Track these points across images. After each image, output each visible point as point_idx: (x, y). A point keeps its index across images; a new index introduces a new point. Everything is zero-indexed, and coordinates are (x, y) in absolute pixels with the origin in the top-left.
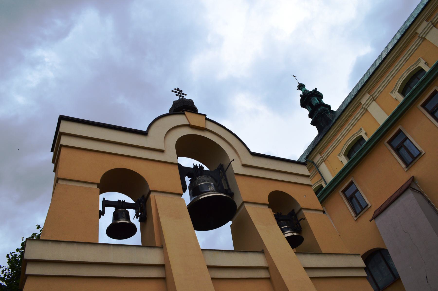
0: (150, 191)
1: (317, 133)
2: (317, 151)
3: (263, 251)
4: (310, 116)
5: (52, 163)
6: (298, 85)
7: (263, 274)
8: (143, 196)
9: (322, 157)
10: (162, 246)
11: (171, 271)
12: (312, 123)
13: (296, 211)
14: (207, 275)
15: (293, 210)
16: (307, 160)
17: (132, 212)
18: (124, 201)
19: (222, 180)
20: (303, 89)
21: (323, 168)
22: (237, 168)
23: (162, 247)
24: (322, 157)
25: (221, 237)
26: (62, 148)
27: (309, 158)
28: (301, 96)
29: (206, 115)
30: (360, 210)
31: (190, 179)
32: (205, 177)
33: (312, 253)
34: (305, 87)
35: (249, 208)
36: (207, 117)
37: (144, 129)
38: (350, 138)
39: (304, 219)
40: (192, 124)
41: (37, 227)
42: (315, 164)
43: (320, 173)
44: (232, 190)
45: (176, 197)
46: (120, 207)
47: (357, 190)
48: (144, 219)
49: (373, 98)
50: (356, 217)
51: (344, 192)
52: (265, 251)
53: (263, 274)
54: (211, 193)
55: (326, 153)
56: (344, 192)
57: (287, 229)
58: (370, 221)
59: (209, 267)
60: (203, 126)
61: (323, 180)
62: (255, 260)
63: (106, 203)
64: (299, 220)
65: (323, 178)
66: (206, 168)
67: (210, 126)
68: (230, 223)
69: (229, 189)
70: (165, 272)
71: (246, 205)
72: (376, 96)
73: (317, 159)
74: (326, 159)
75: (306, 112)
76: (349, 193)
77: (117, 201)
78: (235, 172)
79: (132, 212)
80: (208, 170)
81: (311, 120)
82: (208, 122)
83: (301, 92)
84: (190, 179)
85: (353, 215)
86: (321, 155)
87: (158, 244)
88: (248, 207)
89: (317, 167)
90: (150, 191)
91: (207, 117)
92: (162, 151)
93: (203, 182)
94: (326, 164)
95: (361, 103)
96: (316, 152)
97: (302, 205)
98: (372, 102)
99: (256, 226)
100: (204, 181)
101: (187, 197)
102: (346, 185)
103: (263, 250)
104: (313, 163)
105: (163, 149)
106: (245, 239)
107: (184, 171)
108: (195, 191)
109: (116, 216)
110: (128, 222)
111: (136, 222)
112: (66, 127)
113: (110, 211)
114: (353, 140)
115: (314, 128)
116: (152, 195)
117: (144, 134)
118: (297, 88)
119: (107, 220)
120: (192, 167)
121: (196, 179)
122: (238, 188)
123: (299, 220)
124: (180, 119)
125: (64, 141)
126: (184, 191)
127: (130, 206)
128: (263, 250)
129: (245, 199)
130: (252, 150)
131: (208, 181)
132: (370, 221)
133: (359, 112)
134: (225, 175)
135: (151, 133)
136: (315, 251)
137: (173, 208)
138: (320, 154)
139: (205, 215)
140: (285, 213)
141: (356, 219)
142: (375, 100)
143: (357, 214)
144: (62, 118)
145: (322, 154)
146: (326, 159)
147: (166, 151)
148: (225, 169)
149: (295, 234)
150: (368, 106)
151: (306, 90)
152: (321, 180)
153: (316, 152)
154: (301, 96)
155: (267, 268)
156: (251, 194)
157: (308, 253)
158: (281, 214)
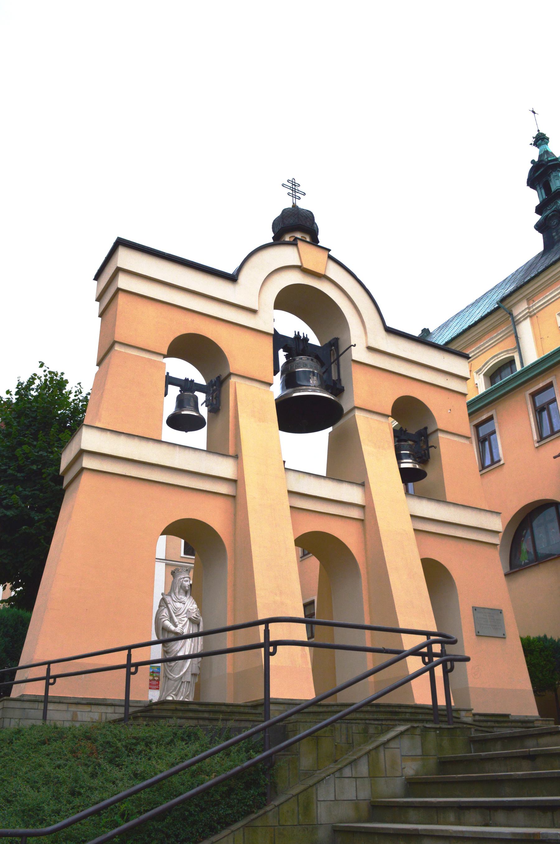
0: (230, 374)
1: (540, 248)
3: (363, 484)
4: (539, 210)
5: (97, 300)
6: (535, 134)
7: (355, 513)
8: (219, 377)
9: (529, 308)
10: (237, 455)
11: (245, 491)
12: (539, 227)
13: (430, 431)
14: (286, 502)
15: (426, 428)
16: (502, 305)
17: (201, 397)
18: (193, 381)
19: (333, 365)
20: (543, 147)
21: (526, 329)
22: (359, 353)
23: (237, 457)
25: (311, 449)
26: (120, 292)
28: (533, 162)
29: (329, 250)
30: (549, 433)
31: (285, 353)
32: (308, 359)
33: (430, 499)
34: (547, 143)
35: (360, 417)
36: (330, 253)
39: (435, 448)
40: (305, 266)
41: (39, 364)
42: (513, 318)
43: (517, 337)
44: (344, 383)
45: (263, 387)
46: (187, 386)
47: (554, 400)
48: (215, 406)
50: (538, 442)
51: (533, 395)
52: (366, 484)
53: (355, 513)
54: (312, 390)
55: (539, 302)
56: (533, 395)
57: (408, 456)
58: (555, 457)
59: (290, 492)
60: (322, 272)
61: (517, 350)
62: (351, 494)
63: (170, 381)
64: (430, 445)
65: (518, 348)
67: (333, 272)
68: (330, 429)
69: (339, 380)
70: (236, 489)
71: (358, 413)
73: (520, 309)
74: (535, 314)
75: (533, 198)
76: (541, 400)
77: (184, 379)
78: (354, 358)
79: (201, 397)
81: (538, 217)
82: (332, 264)
83: (535, 154)
84: (285, 353)
85: (535, 438)
86: (528, 304)
87: (231, 452)
88: (359, 415)
89: (515, 323)
90: (230, 374)
91: (330, 253)
92: (254, 312)
93: (304, 367)
94: (532, 324)
96: (522, 296)
97: (440, 425)
99: (364, 447)
100: (305, 366)
101: (277, 389)
102: (541, 385)
103: (364, 483)
104: (511, 314)
105: (255, 307)
106: (344, 462)
107: (279, 341)
108: (290, 380)
109: (181, 402)
110: (196, 414)
111: (204, 411)
112: (126, 259)
113: (174, 391)
115: (539, 238)
116: (233, 380)
117: (232, 278)
118: (532, 141)
119: (169, 406)
120: (292, 336)
121: (294, 360)
122: (352, 385)
123: (430, 445)
124: (286, 255)
125: (123, 282)
126: (275, 373)
127: (200, 388)
128: (364, 483)
129: (357, 402)
130: (388, 324)
131: (311, 368)
132: (555, 457)
134: (338, 359)
135: (242, 278)
136: (437, 496)
137: (256, 400)
138: (528, 300)
139: (295, 416)
140: (413, 430)
141: (537, 445)
143: (541, 438)
144: (120, 243)
145: (531, 301)
146: (535, 314)
147: (260, 313)
148: (341, 353)
149: (417, 467)
151: (547, 152)
152: (515, 348)
153: (522, 296)
154: (533, 162)
155: (363, 507)
156: (369, 399)
157: (424, 497)
158: (406, 431)
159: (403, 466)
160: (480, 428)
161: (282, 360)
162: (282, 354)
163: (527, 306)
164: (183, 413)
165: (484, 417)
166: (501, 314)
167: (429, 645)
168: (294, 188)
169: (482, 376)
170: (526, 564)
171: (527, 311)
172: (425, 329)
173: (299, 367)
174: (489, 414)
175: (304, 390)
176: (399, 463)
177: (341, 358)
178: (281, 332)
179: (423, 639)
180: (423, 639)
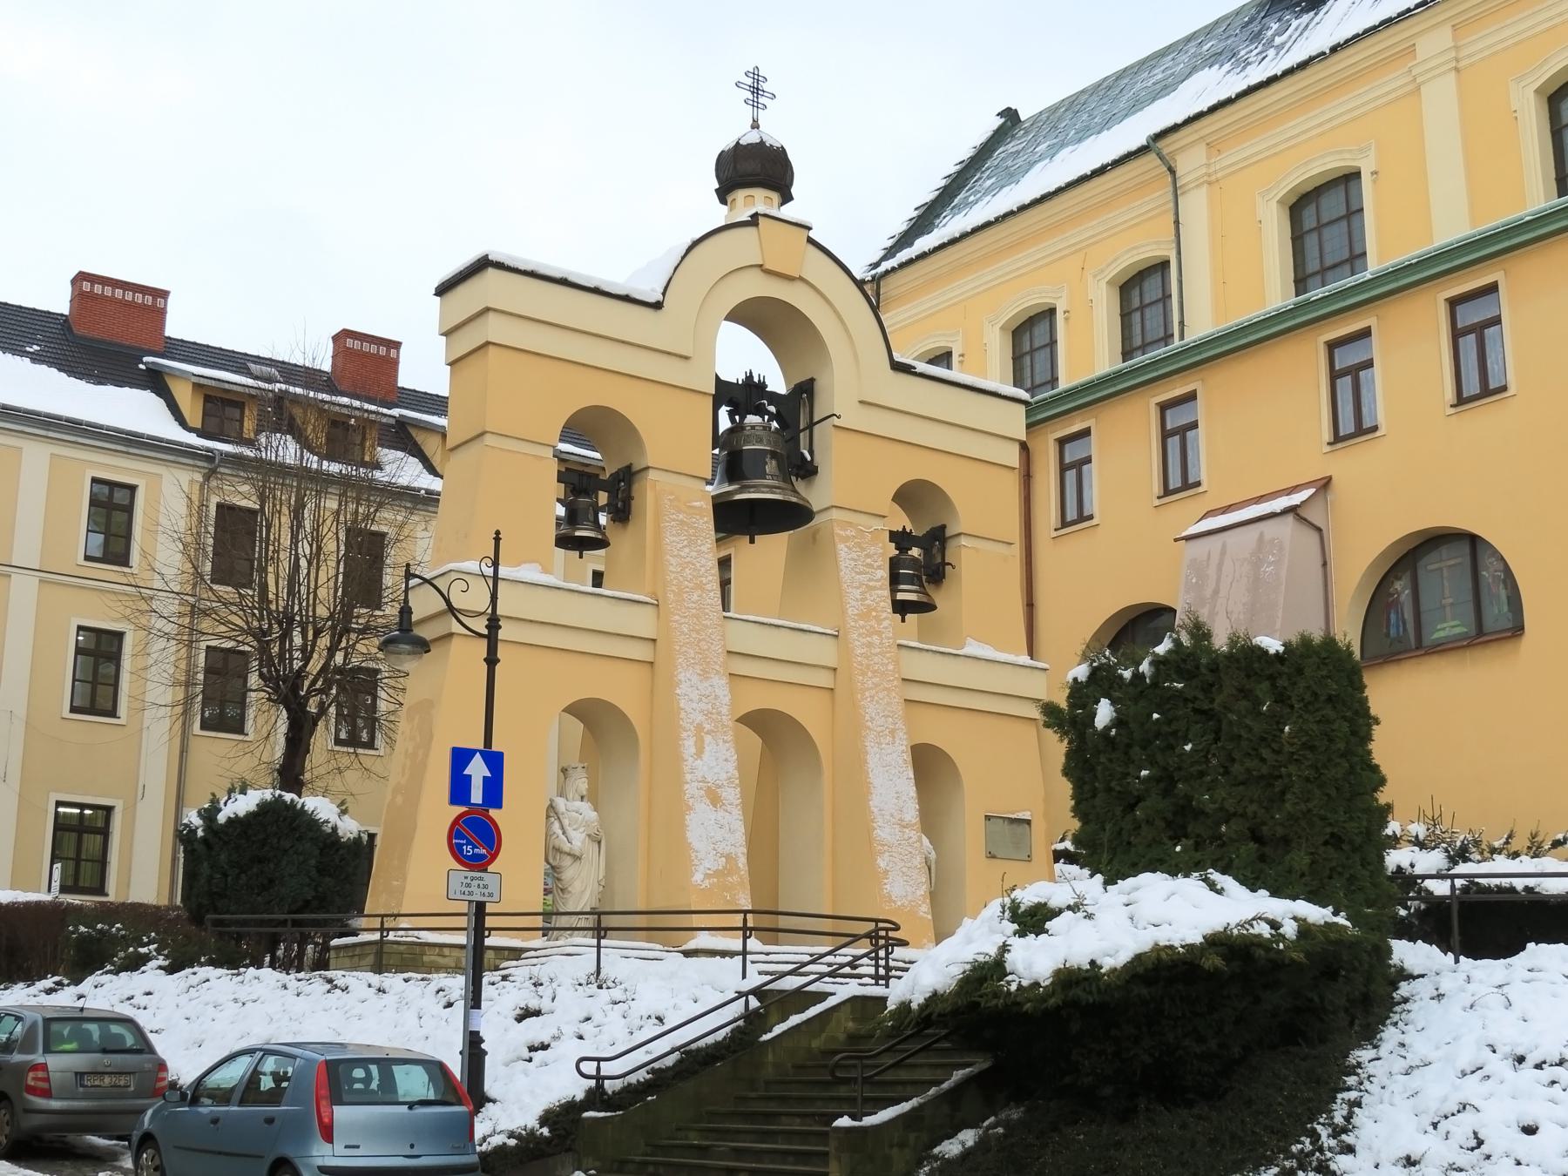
2: (1203, 133)
13: (949, 533)
15: (943, 527)
24: (1208, 165)
27: (1160, 144)
37: (655, 297)
38: (1322, 157)
49: (1457, 60)
55: (1232, 156)
57: (910, 580)
66: (844, 1122)
72: (1469, 56)
80: (836, 1124)
90: (647, 468)
91: (812, 234)
95: (1411, 51)
98: (1444, 73)
114: (1329, 167)
116: (652, 475)
117: (658, 306)
133: (1392, 82)
141: (1157, 502)
142: (1457, 70)
150: (1429, 80)
153: (1196, 136)
159: (900, 596)
160: (1067, 447)
161: (725, 423)
162: (723, 412)
163: (1204, 161)
164: (578, 533)
165: (1076, 427)
166: (1150, 160)
167: (877, 930)
168: (756, 89)
169: (1103, 284)
170: (1470, 332)
171: (1204, 170)
172: (1009, 109)
173: (749, 443)
174: (1083, 425)
175: (757, 488)
176: (894, 591)
177: (816, 428)
178: (723, 378)
179: (872, 926)
180: (872, 926)
